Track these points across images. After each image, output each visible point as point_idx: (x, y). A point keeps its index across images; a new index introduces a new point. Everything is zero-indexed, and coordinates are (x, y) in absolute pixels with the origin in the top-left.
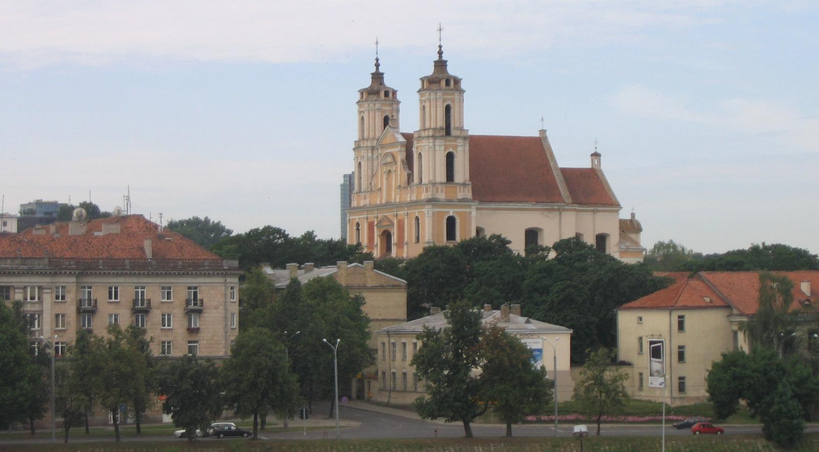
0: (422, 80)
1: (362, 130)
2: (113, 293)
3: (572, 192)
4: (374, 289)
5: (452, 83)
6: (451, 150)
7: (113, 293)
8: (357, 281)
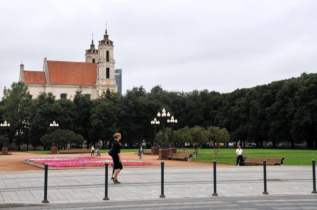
5: (109, 43)
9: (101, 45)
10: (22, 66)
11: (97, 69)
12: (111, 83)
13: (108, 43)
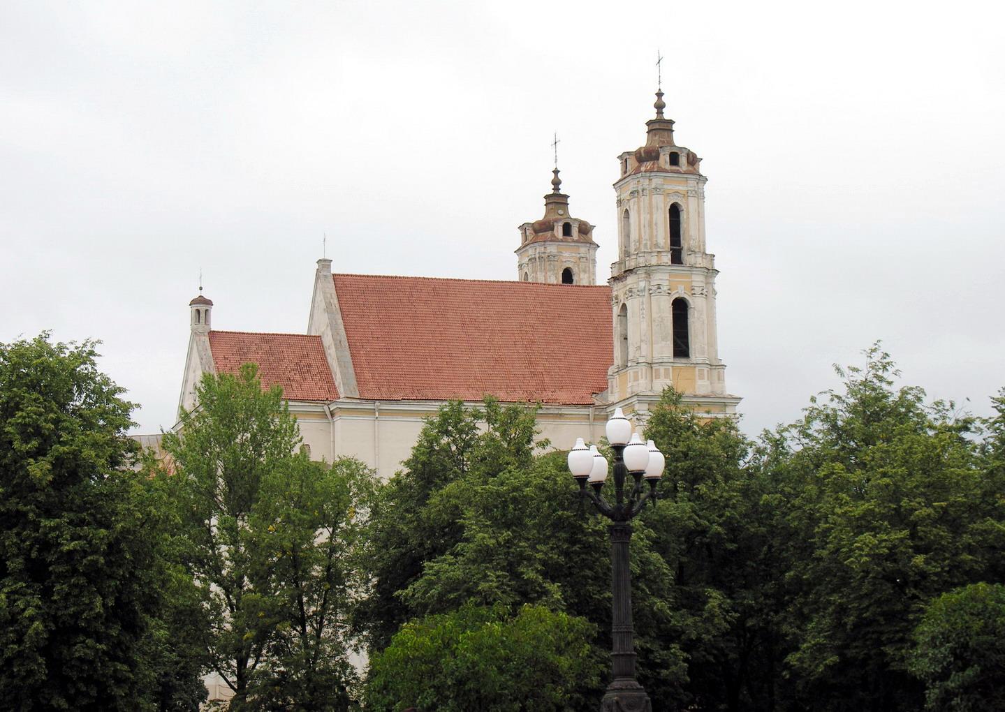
0: (523, 228)
5: (683, 160)
9: (637, 171)
10: (201, 306)
11: (616, 310)
12: (700, 382)
13: (674, 159)
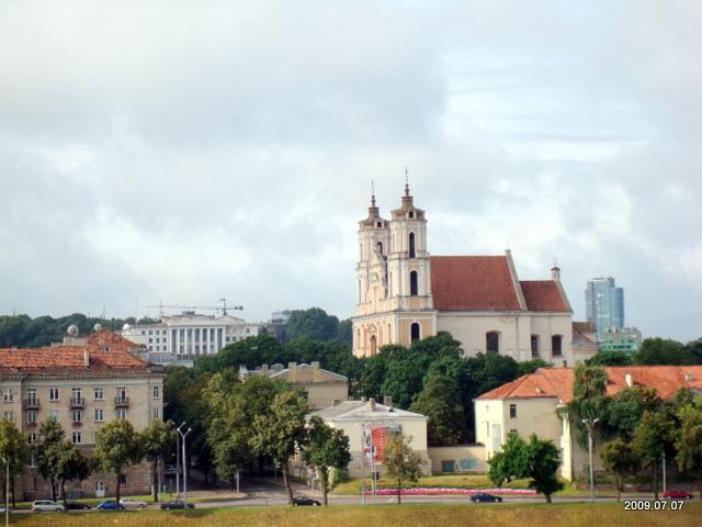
1: (362, 256)
2: (54, 395)
3: (528, 304)
4: (319, 384)
5: (415, 214)
6: (414, 269)
7: (54, 395)
8: (304, 378)
